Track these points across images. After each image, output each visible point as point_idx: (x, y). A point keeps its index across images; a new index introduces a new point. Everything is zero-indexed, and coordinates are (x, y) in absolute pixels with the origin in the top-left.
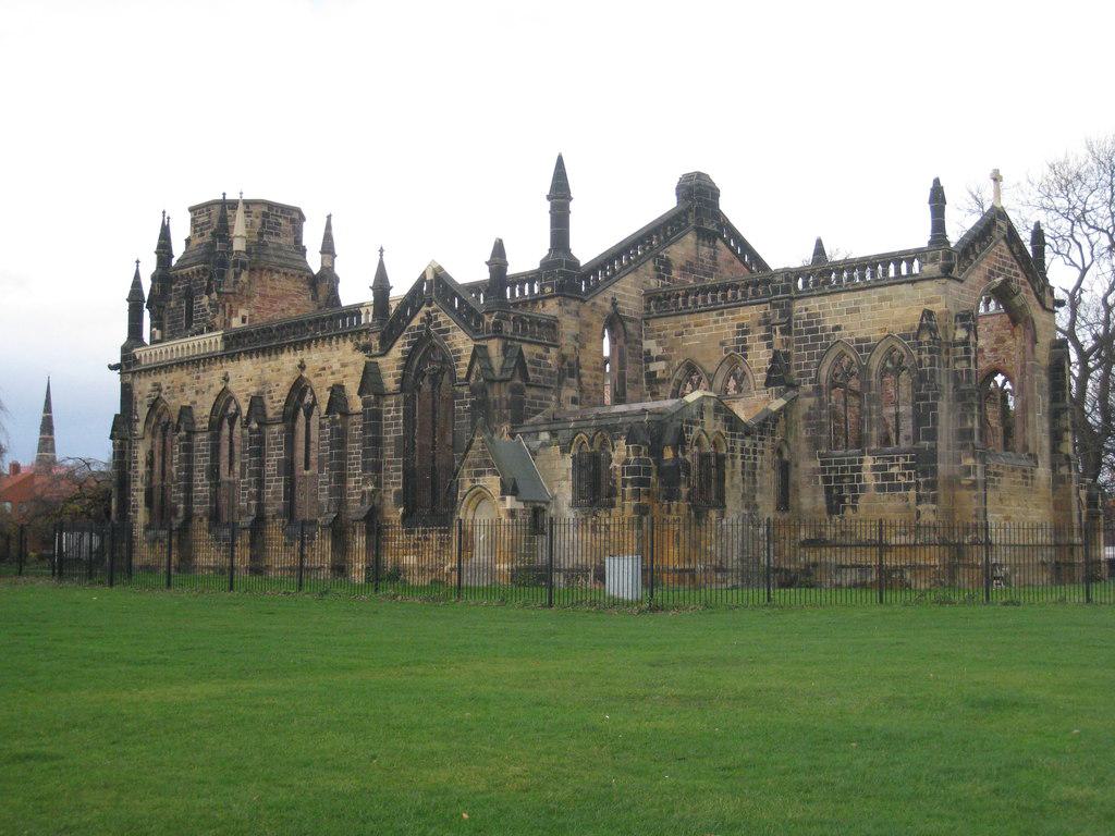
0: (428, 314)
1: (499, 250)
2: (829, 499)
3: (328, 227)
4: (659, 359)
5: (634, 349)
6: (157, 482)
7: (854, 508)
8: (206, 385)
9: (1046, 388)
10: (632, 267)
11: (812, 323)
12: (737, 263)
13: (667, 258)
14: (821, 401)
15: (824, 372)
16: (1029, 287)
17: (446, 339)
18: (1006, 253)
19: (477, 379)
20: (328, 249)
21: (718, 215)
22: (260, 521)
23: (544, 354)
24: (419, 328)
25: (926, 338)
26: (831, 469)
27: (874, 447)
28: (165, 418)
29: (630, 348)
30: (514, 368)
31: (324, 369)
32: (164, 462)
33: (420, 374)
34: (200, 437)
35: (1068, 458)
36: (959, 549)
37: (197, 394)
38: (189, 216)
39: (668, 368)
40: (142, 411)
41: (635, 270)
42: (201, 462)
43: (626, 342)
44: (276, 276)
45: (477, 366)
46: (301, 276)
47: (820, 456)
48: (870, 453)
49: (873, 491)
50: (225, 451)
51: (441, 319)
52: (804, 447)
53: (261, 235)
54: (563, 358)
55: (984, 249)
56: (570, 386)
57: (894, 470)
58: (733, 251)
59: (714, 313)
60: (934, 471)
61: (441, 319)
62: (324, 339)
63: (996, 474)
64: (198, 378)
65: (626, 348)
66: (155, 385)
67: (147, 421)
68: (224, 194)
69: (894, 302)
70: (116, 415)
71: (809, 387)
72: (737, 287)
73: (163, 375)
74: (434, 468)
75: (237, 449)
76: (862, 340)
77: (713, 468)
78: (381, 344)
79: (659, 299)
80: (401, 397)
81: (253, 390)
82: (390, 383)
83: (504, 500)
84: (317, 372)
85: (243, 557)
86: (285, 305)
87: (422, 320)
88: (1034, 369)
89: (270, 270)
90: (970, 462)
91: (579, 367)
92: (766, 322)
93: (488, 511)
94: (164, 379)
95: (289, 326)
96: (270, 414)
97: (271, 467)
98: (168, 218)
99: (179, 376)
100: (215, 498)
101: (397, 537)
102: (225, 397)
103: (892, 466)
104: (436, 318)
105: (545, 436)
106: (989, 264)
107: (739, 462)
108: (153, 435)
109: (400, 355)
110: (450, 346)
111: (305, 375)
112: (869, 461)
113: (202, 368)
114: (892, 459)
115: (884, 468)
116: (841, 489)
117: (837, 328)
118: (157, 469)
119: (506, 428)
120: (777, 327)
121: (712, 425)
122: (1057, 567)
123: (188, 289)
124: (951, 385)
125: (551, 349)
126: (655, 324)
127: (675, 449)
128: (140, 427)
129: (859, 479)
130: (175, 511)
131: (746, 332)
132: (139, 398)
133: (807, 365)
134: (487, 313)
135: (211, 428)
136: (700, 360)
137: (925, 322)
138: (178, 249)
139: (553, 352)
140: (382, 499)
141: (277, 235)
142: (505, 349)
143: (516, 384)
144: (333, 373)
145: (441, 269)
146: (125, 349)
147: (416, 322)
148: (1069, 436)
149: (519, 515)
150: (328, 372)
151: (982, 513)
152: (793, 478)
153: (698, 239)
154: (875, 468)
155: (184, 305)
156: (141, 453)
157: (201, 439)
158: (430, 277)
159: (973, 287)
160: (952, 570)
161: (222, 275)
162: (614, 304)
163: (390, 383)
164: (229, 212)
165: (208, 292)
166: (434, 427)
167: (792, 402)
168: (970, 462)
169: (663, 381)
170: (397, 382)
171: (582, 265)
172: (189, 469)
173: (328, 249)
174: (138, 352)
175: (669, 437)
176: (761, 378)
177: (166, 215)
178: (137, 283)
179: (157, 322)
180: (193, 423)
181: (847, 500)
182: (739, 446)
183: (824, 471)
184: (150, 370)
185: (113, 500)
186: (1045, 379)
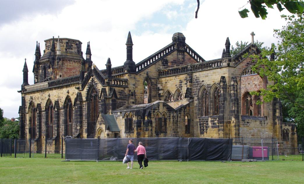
0: (92, 79)
1: (109, 61)
2: (201, 131)
3: (89, 46)
4: (161, 90)
5: (154, 87)
7: (206, 132)
8: (44, 97)
10: (154, 63)
12: (192, 59)
13: (166, 59)
15: (200, 94)
17: (96, 86)
19: (103, 98)
23: (123, 90)
24: (91, 83)
25: (222, 84)
26: (201, 121)
27: (211, 115)
29: (153, 87)
30: (113, 94)
31: (74, 93)
34: (43, 113)
37: (41, 99)
38: (44, 43)
40: (28, 105)
42: (44, 120)
43: (151, 85)
44: (71, 62)
45: (103, 94)
46: (79, 62)
47: (199, 118)
48: (210, 117)
49: (211, 128)
51: (95, 81)
54: (130, 91)
56: (132, 98)
59: (174, 76)
61: (95, 81)
63: (248, 123)
64: (42, 95)
65: (152, 87)
66: (31, 97)
67: (29, 108)
68: (53, 37)
69: (216, 74)
70: (20, 106)
73: (33, 94)
79: (161, 72)
80: (87, 103)
81: (56, 99)
82: (84, 99)
83: (106, 131)
84: (72, 94)
86: (74, 71)
87: (91, 81)
89: (69, 60)
91: (135, 93)
92: (186, 79)
94: (33, 95)
96: (61, 106)
97: (61, 122)
98: (39, 44)
99: (37, 95)
102: (49, 101)
103: (215, 121)
105: (119, 113)
106: (247, 61)
107: (172, 120)
109: (86, 91)
111: (69, 95)
112: (210, 119)
113: (43, 92)
114: (215, 119)
115: (213, 121)
116: (203, 127)
117: (203, 81)
118: (32, 122)
120: (188, 81)
121: (162, 109)
123: (44, 67)
124: (229, 97)
125: (126, 88)
128: (27, 110)
130: (37, 134)
131: (181, 82)
133: (196, 92)
134: (106, 79)
137: (221, 80)
138: (42, 53)
139: (126, 89)
141: (72, 49)
142: (110, 89)
143: (113, 99)
145: (96, 66)
146: (22, 86)
147: (90, 81)
152: (191, 124)
153: (178, 53)
155: (43, 71)
156: (28, 117)
157: (44, 113)
161: (54, 62)
163: (84, 99)
164: (55, 42)
165: (50, 68)
166: (95, 110)
169: (162, 96)
170: (85, 98)
171: (136, 64)
173: (89, 52)
174: (26, 87)
177: (38, 43)
178: (26, 67)
180: (41, 109)
184: (30, 92)
185: (20, 132)
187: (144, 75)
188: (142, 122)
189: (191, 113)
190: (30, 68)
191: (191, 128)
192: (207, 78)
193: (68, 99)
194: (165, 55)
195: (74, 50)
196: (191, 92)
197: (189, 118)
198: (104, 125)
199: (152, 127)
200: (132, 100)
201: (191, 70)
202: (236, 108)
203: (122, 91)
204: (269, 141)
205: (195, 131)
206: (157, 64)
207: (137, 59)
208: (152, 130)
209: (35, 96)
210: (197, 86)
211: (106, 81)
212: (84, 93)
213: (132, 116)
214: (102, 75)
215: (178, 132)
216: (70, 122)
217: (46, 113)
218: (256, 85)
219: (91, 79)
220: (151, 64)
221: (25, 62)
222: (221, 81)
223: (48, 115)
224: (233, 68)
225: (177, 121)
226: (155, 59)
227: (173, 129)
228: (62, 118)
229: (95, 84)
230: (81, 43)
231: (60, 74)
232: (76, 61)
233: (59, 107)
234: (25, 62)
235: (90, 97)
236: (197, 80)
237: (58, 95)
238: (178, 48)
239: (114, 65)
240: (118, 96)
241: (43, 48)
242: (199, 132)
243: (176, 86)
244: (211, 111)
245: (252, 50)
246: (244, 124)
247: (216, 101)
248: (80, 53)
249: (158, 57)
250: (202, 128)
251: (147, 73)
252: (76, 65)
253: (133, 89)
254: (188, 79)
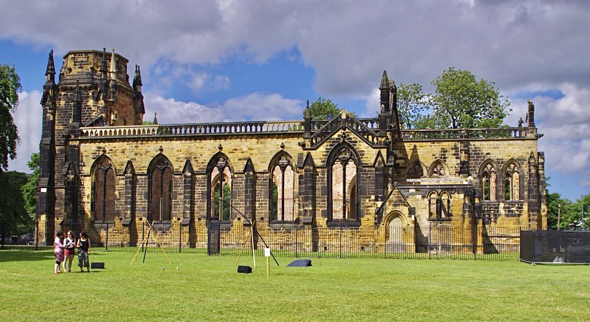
4: (401, 158)
7: (495, 222)
11: (477, 151)
39: (406, 163)
49: (504, 216)
57: (514, 209)
69: (514, 147)
73: (107, 144)
76: (500, 160)
85: (145, 246)
94: (108, 146)
104: (348, 135)
110: (357, 148)
112: (502, 205)
115: (509, 208)
117: (488, 154)
129: (498, 211)
131: (446, 151)
132: (85, 154)
144: (242, 152)
181: (492, 219)
192: (497, 150)
204: (423, 255)
209: (115, 147)
210: (478, 160)
217: (149, 179)
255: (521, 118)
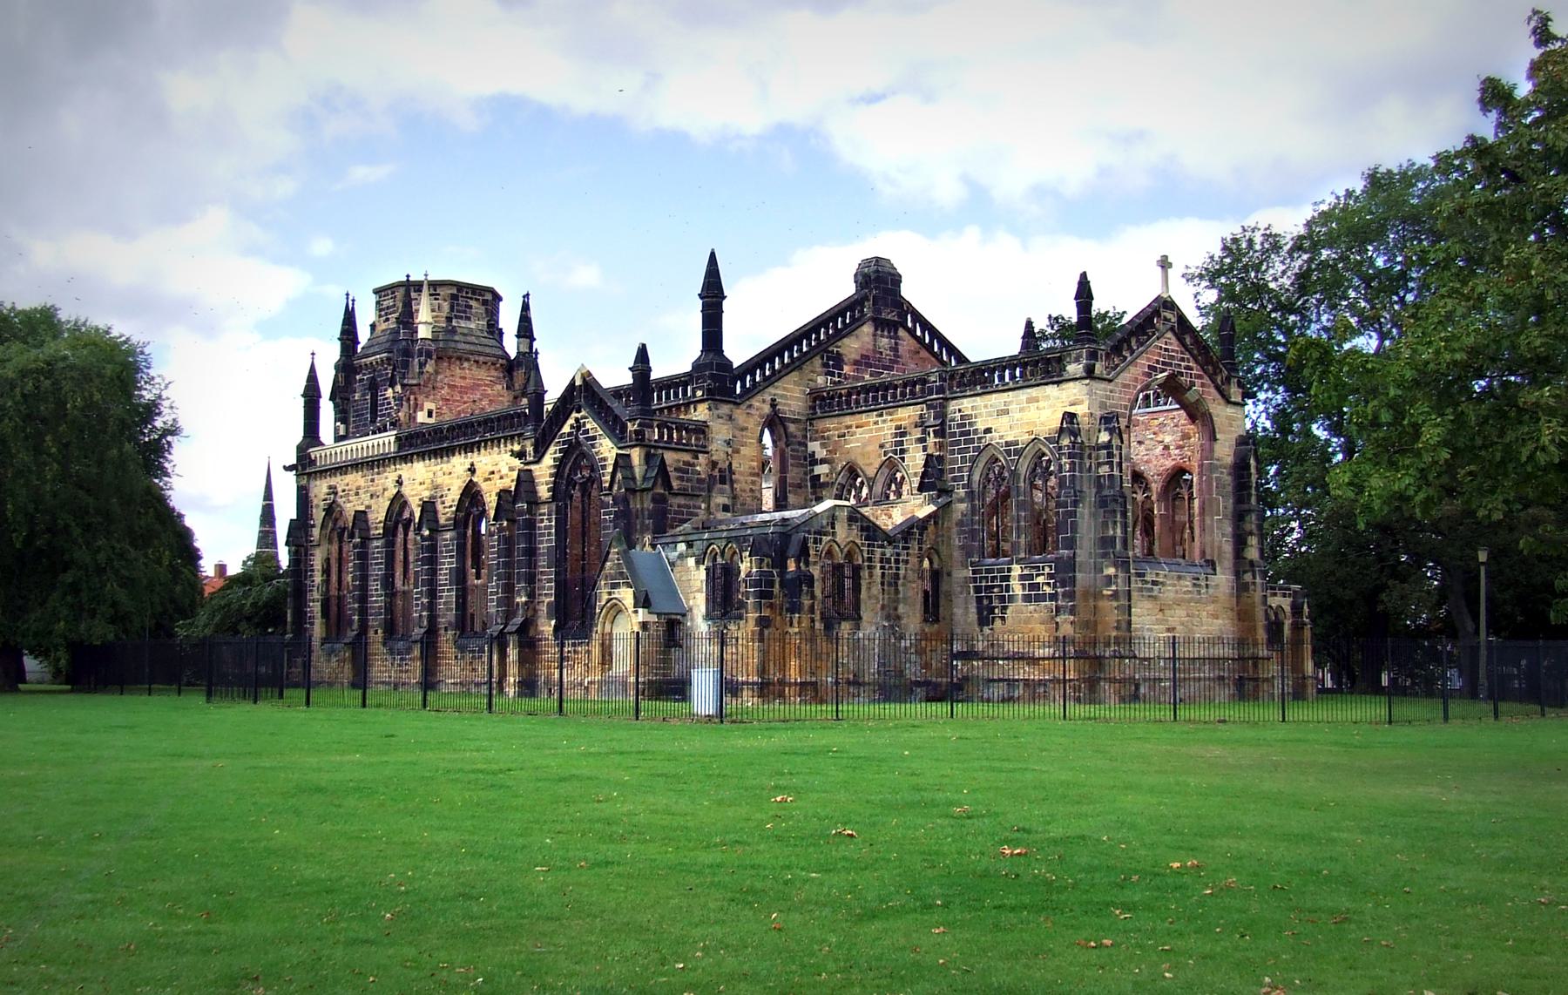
0: (577, 420)
1: (643, 354)
2: (980, 612)
3: (526, 307)
4: (823, 461)
6: (333, 592)
7: (1003, 619)
9: (1230, 489)
10: (796, 365)
12: (924, 354)
14: (973, 506)
15: (976, 477)
16: (1206, 380)
17: (593, 446)
18: (1174, 345)
20: (525, 330)
21: (904, 308)
22: (432, 631)
24: (570, 434)
25: (1065, 442)
27: (1022, 555)
28: (341, 523)
32: (340, 571)
33: (571, 483)
34: (375, 543)
35: (1252, 563)
36: (1098, 662)
37: (367, 496)
38: (373, 298)
40: (318, 515)
41: (799, 368)
42: (377, 571)
44: (466, 365)
45: (619, 476)
49: (1020, 603)
50: (400, 556)
51: (588, 426)
52: (957, 554)
53: (449, 319)
54: (714, 464)
55: (1142, 344)
56: (722, 492)
57: (1040, 580)
58: (920, 340)
60: (1073, 581)
61: (588, 426)
62: (492, 440)
63: (1154, 583)
69: (1041, 404)
71: (962, 492)
72: (896, 387)
73: (339, 478)
74: (583, 580)
75: (411, 558)
77: (846, 577)
78: (536, 451)
79: (823, 399)
80: (554, 507)
81: (426, 494)
82: (544, 492)
87: (572, 427)
88: (1212, 468)
89: (460, 359)
90: (1111, 571)
91: (732, 472)
92: (921, 423)
93: (625, 622)
94: (340, 482)
95: (459, 426)
96: (442, 521)
97: (443, 576)
99: (354, 479)
100: (390, 608)
101: (550, 651)
102: (399, 502)
105: (682, 547)
106: (1148, 359)
107: (878, 572)
108: (330, 541)
112: (1016, 570)
115: (1031, 577)
117: (988, 431)
118: (334, 578)
119: (647, 538)
121: (844, 534)
122: (1240, 683)
126: (820, 425)
127: (798, 562)
128: (316, 532)
129: (1008, 588)
130: (351, 622)
131: (903, 434)
133: (960, 470)
135: (385, 535)
136: (861, 462)
138: (364, 335)
140: (535, 611)
141: (468, 319)
142: (648, 458)
145: (589, 374)
147: (566, 429)
148: (1253, 541)
149: (652, 628)
150: (497, 476)
151: (1124, 625)
152: (944, 587)
154: (1022, 577)
156: (317, 561)
158: (578, 383)
159: (1125, 386)
160: (1093, 684)
161: (406, 365)
162: (773, 404)
163: (544, 492)
164: (413, 295)
165: (392, 385)
167: (945, 509)
168: (1111, 571)
169: (825, 485)
172: (364, 578)
173: (525, 330)
174: (314, 452)
175: (793, 548)
176: (916, 481)
178: (312, 379)
179: (342, 415)
180: (368, 529)
182: (878, 556)
183: (975, 580)
186: (1227, 479)
187: (761, 406)
188: (777, 580)
189: (943, 549)
190: (326, 386)
191: (942, 602)
192: (1005, 419)
193: (471, 494)
194: (833, 336)
195: (476, 324)
196: (942, 471)
197: (935, 566)
198: (630, 591)
199: (813, 597)
200: (720, 500)
201: (941, 390)
202: (1119, 531)
203: (687, 463)
205: (958, 611)
206: (807, 367)
207: (739, 348)
208: (812, 610)
210: (966, 450)
211: (631, 427)
212: (544, 471)
213: (736, 557)
214: (615, 405)
215: (898, 618)
216: (478, 577)
218: (1166, 448)
219: (571, 421)
220: (787, 369)
221: (313, 366)
222: (1061, 430)
223: (393, 552)
224: (1103, 385)
225: (897, 576)
226: (800, 350)
227: (883, 607)
228: (447, 564)
229: (588, 439)
230: (500, 299)
231: (429, 405)
232: (481, 359)
233: (437, 521)
234: (313, 366)
235: (568, 485)
236: (964, 425)
237: (433, 480)
238: (877, 311)
239: (660, 369)
240: (675, 484)
241: (366, 317)
242: (973, 615)
243: (882, 446)
244: (1022, 540)
245: (1165, 319)
246: (1141, 590)
247: (1012, 511)
248: (495, 332)
249: (809, 344)
250: (985, 602)
251: (773, 400)
252: (482, 374)
253: (723, 456)
254: (932, 421)
255: (1029, 324)
